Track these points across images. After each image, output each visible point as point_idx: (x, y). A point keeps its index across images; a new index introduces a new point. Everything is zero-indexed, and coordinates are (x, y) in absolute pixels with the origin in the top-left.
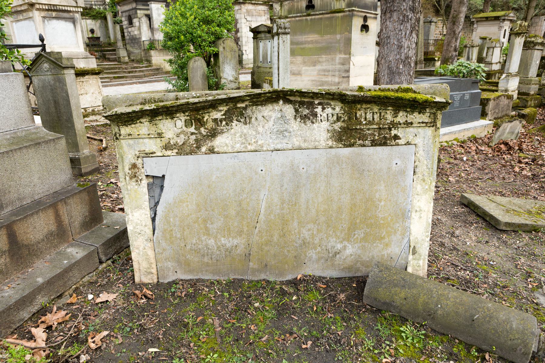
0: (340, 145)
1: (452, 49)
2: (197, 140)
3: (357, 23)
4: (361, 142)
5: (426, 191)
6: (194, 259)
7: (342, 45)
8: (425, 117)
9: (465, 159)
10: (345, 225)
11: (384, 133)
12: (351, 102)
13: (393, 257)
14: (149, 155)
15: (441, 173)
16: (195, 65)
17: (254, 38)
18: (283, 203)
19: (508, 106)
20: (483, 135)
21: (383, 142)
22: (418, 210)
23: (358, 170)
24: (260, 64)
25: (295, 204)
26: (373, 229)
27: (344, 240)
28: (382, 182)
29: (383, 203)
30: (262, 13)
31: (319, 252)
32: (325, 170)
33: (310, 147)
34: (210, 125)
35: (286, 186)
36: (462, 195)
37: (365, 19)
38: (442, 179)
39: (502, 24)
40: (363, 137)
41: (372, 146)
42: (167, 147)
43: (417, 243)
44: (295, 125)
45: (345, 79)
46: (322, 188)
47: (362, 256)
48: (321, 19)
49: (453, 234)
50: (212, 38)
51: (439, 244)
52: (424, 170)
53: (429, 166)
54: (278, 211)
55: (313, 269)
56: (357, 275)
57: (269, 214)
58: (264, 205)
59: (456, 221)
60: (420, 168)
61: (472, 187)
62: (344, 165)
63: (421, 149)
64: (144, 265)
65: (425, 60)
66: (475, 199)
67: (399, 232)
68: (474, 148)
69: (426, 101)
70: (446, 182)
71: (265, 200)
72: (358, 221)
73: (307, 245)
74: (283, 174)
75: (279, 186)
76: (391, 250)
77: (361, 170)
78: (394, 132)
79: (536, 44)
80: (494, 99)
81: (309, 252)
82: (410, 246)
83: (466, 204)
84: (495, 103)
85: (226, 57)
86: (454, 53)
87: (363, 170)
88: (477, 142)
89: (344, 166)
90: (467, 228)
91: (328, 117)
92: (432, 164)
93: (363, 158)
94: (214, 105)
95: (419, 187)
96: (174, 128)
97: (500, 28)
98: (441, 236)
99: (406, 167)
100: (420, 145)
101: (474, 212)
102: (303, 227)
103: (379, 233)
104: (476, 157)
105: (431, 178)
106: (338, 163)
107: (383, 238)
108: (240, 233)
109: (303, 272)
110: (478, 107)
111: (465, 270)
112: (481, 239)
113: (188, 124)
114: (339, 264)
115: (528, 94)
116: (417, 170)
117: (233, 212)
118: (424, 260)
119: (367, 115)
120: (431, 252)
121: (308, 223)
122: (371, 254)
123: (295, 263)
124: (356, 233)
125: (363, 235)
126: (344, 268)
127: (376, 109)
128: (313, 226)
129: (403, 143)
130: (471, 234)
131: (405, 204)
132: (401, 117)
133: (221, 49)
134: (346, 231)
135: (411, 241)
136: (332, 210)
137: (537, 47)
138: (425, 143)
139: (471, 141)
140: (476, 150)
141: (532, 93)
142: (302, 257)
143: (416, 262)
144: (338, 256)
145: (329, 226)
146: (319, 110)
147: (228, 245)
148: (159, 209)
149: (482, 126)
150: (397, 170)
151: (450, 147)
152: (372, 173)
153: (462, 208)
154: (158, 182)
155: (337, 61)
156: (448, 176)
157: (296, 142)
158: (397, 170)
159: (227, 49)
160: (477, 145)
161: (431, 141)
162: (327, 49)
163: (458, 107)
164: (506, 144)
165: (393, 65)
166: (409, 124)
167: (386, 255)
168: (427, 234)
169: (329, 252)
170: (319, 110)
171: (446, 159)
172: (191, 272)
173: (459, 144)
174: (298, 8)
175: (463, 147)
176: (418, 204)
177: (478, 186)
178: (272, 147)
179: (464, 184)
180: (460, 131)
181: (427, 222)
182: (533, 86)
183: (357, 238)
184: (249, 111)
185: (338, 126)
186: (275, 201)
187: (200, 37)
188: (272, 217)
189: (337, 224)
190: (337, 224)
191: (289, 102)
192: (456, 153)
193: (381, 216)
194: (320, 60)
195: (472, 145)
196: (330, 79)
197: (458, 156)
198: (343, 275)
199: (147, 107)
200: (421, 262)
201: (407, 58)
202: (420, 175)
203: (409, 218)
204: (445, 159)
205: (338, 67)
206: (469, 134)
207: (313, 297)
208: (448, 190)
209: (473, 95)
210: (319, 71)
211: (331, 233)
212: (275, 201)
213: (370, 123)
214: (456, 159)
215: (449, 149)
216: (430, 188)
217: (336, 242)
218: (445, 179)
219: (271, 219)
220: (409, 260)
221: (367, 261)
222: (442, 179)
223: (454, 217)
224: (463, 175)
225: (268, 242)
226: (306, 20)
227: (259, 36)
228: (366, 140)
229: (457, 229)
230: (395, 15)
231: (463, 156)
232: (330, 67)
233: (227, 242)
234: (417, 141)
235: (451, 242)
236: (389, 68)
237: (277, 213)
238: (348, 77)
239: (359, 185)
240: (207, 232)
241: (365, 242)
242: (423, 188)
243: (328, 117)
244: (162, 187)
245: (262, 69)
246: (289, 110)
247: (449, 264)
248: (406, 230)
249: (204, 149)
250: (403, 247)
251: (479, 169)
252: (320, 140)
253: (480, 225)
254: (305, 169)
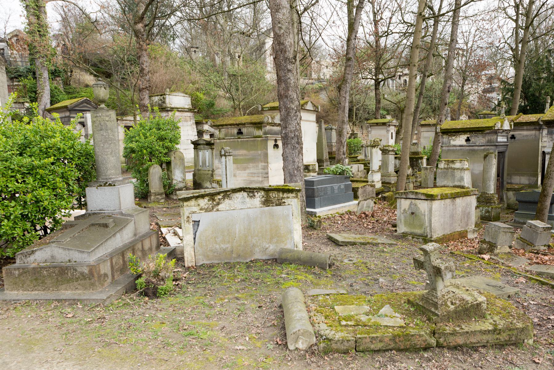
1: (342, 153)
2: (212, 207)
3: (271, 144)
6: (210, 254)
7: (262, 157)
8: (294, 195)
11: (280, 201)
12: (267, 191)
14: (194, 213)
16: (154, 171)
17: (194, 148)
19: (373, 191)
21: (280, 204)
24: (200, 168)
30: (188, 119)
32: (260, 216)
34: (217, 201)
37: (276, 141)
39: (388, 129)
40: (273, 203)
42: (201, 209)
44: (248, 200)
45: (266, 179)
48: (248, 141)
50: (166, 151)
55: (258, 256)
58: (237, 230)
64: (190, 258)
65: (330, 158)
69: (293, 189)
71: (238, 229)
76: (289, 246)
78: (283, 201)
79: (389, 151)
80: (362, 188)
84: (363, 190)
85: (176, 164)
86: (343, 156)
91: (259, 197)
94: (219, 193)
96: (204, 202)
97: (388, 131)
108: (229, 242)
110: (352, 193)
113: (209, 201)
115: (390, 183)
117: (226, 234)
119: (273, 195)
127: (276, 193)
132: (285, 195)
133: (173, 158)
137: (390, 153)
141: (393, 182)
146: (256, 194)
147: (224, 247)
148: (197, 234)
154: (196, 223)
155: (260, 167)
157: (249, 206)
159: (177, 158)
162: (253, 160)
164: (365, 213)
165: (291, 171)
166: (288, 198)
170: (256, 194)
172: (209, 260)
174: (231, 133)
175: (341, 217)
178: (240, 208)
182: (392, 178)
184: (231, 195)
185: (263, 199)
187: (157, 150)
191: (246, 191)
194: (249, 166)
196: (256, 179)
199: (195, 195)
201: (298, 167)
205: (261, 171)
206: (346, 209)
207: (259, 264)
209: (347, 187)
210: (248, 173)
213: (274, 198)
214: (334, 223)
226: (238, 141)
227: (199, 147)
230: (289, 146)
232: (255, 171)
233: (224, 246)
234: (292, 203)
236: (289, 173)
238: (268, 177)
240: (216, 243)
243: (259, 197)
244: (198, 225)
245: (202, 172)
246: (245, 194)
248: (292, 238)
249: (215, 210)
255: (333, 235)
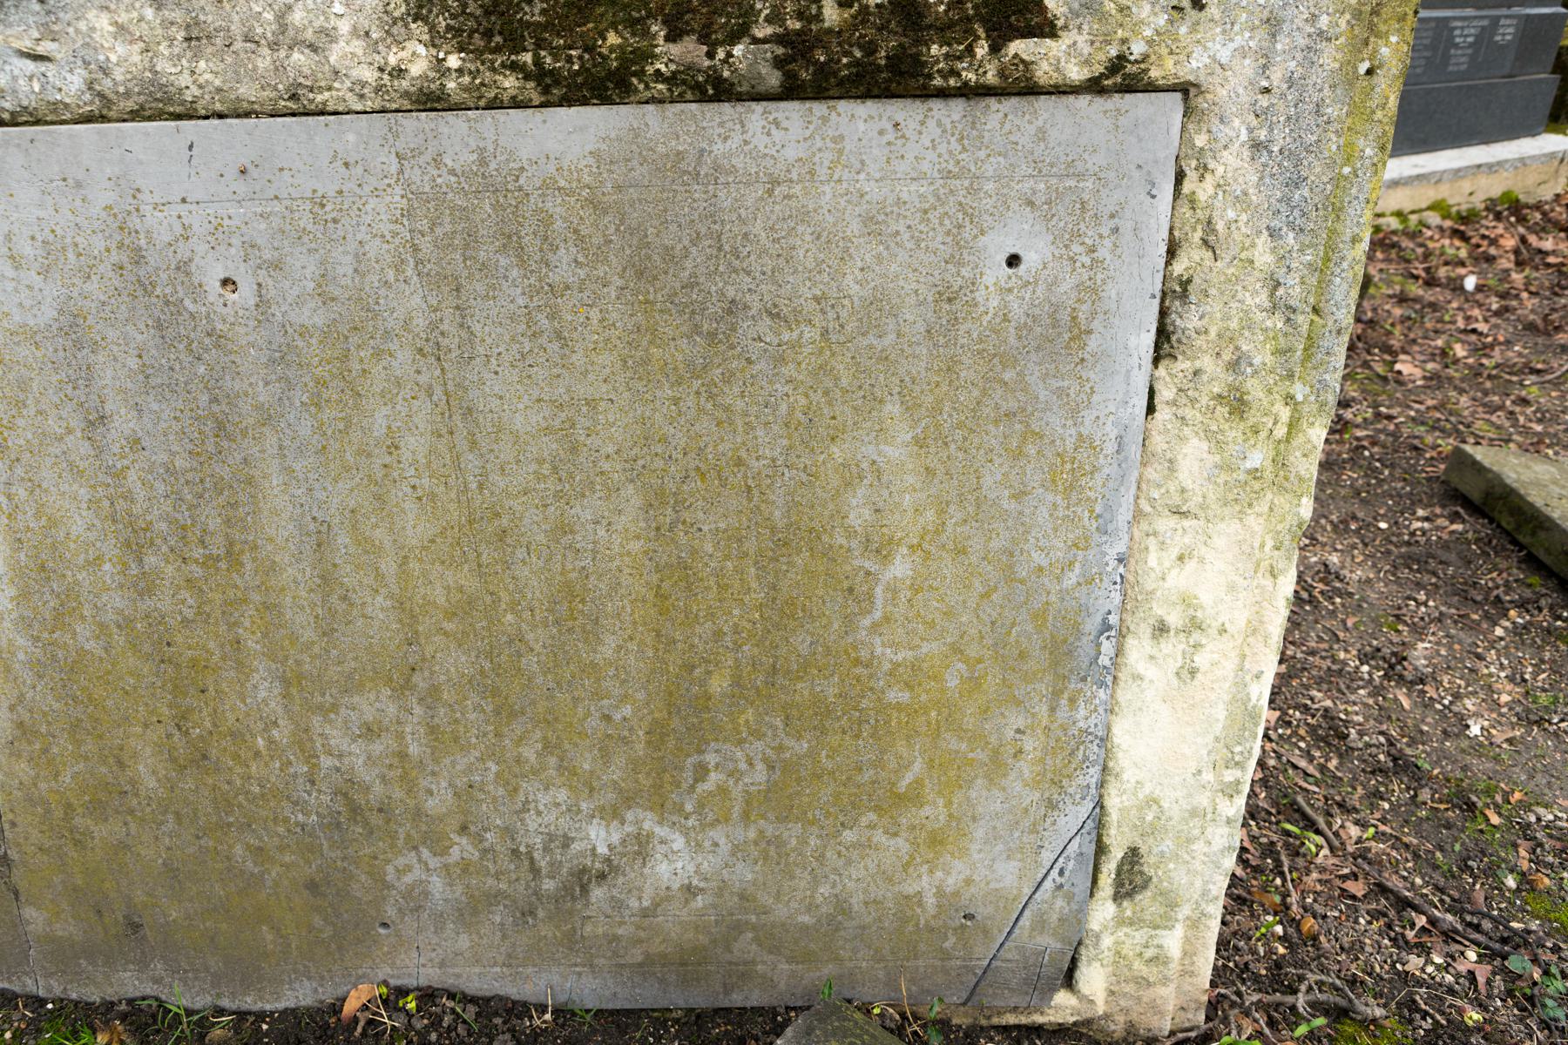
0: (510, 83)
4: (689, 50)
5: (1243, 491)
9: (1470, 283)
10: (627, 710)
13: (981, 912)
15: (1368, 339)
18: (136, 542)
20: (1547, 194)
22: (1174, 619)
23: (689, 299)
25: (233, 557)
26: (834, 740)
27: (628, 799)
28: (893, 408)
29: (900, 568)
31: (465, 867)
32: (411, 303)
33: (248, 91)
35: (123, 423)
36: (1458, 452)
38: (1366, 365)
41: (791, 91)
43: (1152, 831)
46: (415, 445)
47: (766, 899)
49: (1394, 665)
51: (1312, 730)
52: (1248, 324)
53: (1293, 289)
54: (116, 601)
56: (736, 1000)
57: (60, 619)
59: (1419, 585)
60: (1214, 307)
61: (1501, 407)
62: (564, 256)
63: (1239, 129)
66: (1526, 476)
67: (1025, 767)
68: (1509, 243)
70: (1385, 379)
72: (719, 684)
73: (376, 820)
74: (72, 327)
75: (76, 422)
77: (715, 308)
81: (401, 861)
82: (1101, 849)
83: (1476, 496)
87: (733, 308)
88: (1522, 220)
89: (564, 266)
90: (1473, 627)
92: (1322, 272)
93: (725, 199)
95: (1193, 460)
98: (1335, 679)
99: (1091, 291)
100: (1231, 90)
101: (1514, 542)
102: (327, 711)
103: (878, 764)
104: (1517, 278)
105: (1299, 391)
106: (510, 241)
107: (914, 797)
109: (384, 972)
111: (1449, 936)
112: (1544, 699)
114: (616, 938)
116: (1187, 321)
118: (1194, 924)
120: (1264, 782)
121: (352, 685)
122: (824, 890)
123: (318, 921)
124: (711, 759)
125: (760, 774)
126: (649, 960)
128: (392, 709)
129: (1076, 73)
130: (1494, 668)
131: (1071, 579)
134: (640, 749)
135: (1113, 816)
136: (513, 607)
138: (1277, 77)
139: (1498, 217)
140: (1516, 252)
142: (356, 890)
143: (1139, 936)
144: (598, 893)
145: (505, 712)
149: (1552, 155)
150: (1017, 310)
151: (1413, 235)
152: (809, 334)
153: (1455, 517)
156: (1394, 354)
158: (1017, 310)
160: (1521, 230)
161: (1330, 58)
163: (1462, 76)
167: (930, 901)
168: (1230, 776)
169: (535, 871)
171: (1389, 284)
173: (1448, 224)
175: (1464, 238)
176: (1178, 580)
177: (1524, 402)
179: (1461, 391)
180: (1458, 174)
181: (1240, 700)
183: (722, 791)
186: (77, 527)
188: (84, 635)
189: (562, 697)
190: (562, 697)
192: (1434, 261)
193: (886, 654)
195: (1500, 230)
197: (1442, 272)
198: (646, 996)
200: (1173, 941)
202: (1207, 362)
203: (1111, 676)
204: (1390, 282)
206: (1494, 187)
208: (1390, 418)
211: (529, 753)
212: (77, 527)
214: (1431, 282)
215: (1406, 243)
216: (1280, 462)
217: (573, 810)
218: (1380, 369)
219: (82, 652)
220: (1094, 925)
221: (805, 929)
222: (1366, 365)
223: (1408, 561)
224: (1460, 351)
225: (109, 797)
228: (733, 38)
229: (1419, 631)
231: (1462, 271)
235: (1384, 714)
237: (110, 616)
239: (705, 425)
241: (782, 819)
242: (1228, 467)
247: (1357, 888)
250: (1047, 857)
251: (1531, 327)
252: (329, 35)
253: (1544, 618)
254: (245, 295)
255: (1516, 468)
